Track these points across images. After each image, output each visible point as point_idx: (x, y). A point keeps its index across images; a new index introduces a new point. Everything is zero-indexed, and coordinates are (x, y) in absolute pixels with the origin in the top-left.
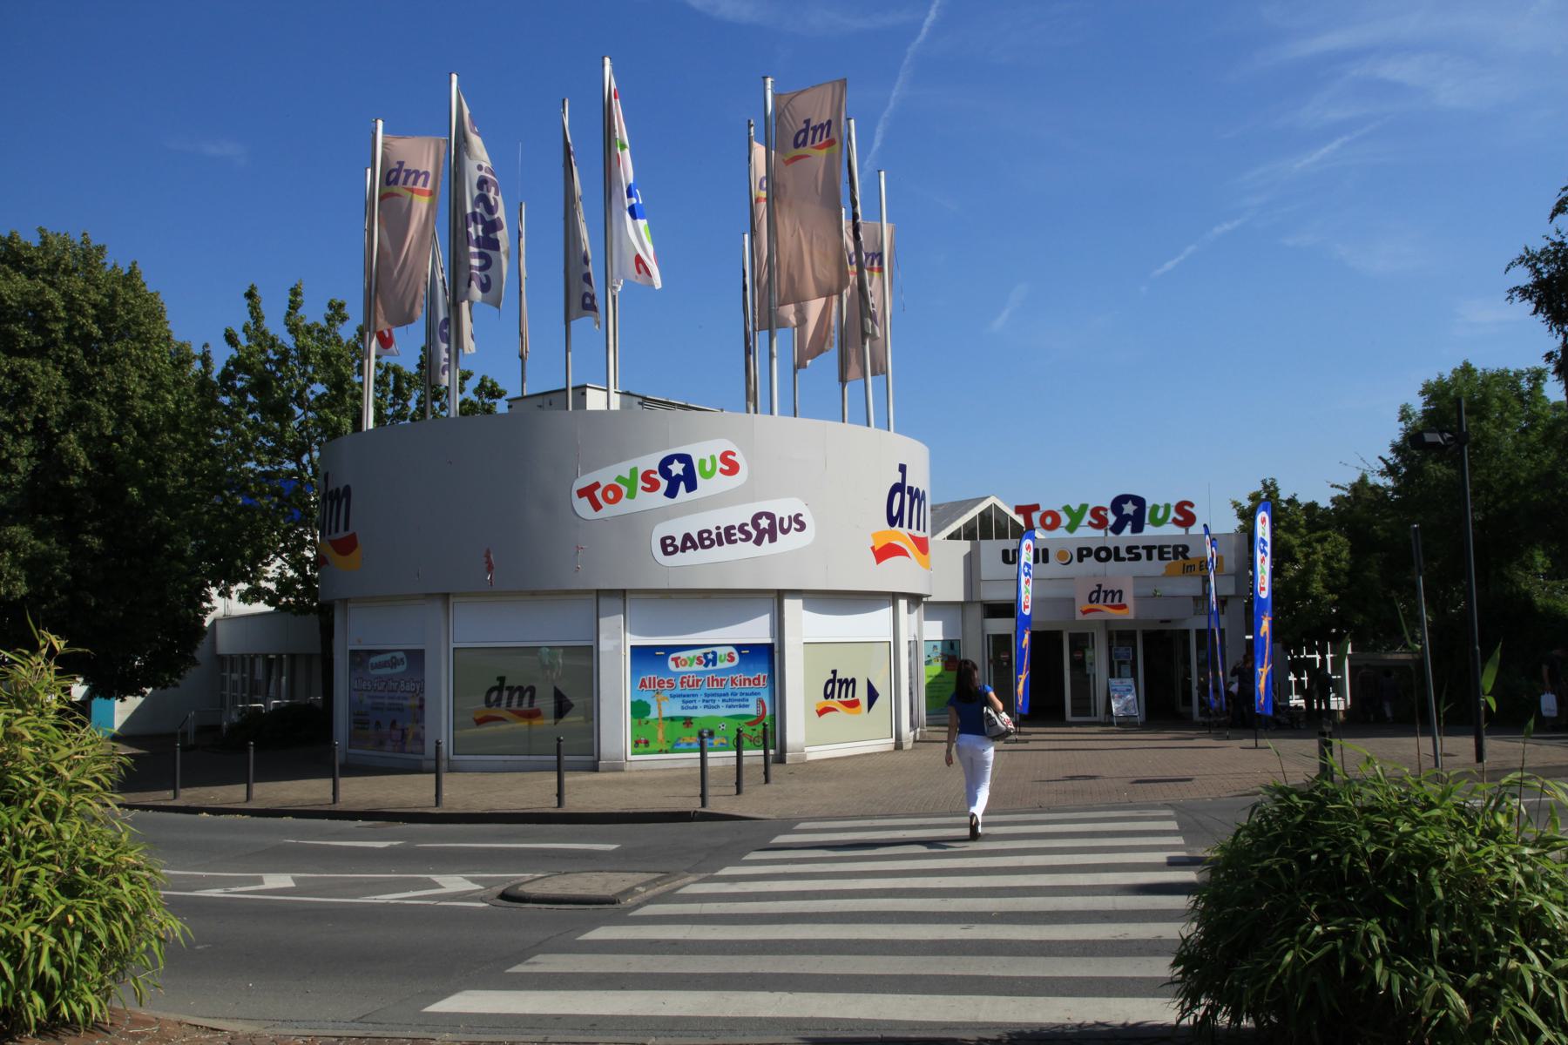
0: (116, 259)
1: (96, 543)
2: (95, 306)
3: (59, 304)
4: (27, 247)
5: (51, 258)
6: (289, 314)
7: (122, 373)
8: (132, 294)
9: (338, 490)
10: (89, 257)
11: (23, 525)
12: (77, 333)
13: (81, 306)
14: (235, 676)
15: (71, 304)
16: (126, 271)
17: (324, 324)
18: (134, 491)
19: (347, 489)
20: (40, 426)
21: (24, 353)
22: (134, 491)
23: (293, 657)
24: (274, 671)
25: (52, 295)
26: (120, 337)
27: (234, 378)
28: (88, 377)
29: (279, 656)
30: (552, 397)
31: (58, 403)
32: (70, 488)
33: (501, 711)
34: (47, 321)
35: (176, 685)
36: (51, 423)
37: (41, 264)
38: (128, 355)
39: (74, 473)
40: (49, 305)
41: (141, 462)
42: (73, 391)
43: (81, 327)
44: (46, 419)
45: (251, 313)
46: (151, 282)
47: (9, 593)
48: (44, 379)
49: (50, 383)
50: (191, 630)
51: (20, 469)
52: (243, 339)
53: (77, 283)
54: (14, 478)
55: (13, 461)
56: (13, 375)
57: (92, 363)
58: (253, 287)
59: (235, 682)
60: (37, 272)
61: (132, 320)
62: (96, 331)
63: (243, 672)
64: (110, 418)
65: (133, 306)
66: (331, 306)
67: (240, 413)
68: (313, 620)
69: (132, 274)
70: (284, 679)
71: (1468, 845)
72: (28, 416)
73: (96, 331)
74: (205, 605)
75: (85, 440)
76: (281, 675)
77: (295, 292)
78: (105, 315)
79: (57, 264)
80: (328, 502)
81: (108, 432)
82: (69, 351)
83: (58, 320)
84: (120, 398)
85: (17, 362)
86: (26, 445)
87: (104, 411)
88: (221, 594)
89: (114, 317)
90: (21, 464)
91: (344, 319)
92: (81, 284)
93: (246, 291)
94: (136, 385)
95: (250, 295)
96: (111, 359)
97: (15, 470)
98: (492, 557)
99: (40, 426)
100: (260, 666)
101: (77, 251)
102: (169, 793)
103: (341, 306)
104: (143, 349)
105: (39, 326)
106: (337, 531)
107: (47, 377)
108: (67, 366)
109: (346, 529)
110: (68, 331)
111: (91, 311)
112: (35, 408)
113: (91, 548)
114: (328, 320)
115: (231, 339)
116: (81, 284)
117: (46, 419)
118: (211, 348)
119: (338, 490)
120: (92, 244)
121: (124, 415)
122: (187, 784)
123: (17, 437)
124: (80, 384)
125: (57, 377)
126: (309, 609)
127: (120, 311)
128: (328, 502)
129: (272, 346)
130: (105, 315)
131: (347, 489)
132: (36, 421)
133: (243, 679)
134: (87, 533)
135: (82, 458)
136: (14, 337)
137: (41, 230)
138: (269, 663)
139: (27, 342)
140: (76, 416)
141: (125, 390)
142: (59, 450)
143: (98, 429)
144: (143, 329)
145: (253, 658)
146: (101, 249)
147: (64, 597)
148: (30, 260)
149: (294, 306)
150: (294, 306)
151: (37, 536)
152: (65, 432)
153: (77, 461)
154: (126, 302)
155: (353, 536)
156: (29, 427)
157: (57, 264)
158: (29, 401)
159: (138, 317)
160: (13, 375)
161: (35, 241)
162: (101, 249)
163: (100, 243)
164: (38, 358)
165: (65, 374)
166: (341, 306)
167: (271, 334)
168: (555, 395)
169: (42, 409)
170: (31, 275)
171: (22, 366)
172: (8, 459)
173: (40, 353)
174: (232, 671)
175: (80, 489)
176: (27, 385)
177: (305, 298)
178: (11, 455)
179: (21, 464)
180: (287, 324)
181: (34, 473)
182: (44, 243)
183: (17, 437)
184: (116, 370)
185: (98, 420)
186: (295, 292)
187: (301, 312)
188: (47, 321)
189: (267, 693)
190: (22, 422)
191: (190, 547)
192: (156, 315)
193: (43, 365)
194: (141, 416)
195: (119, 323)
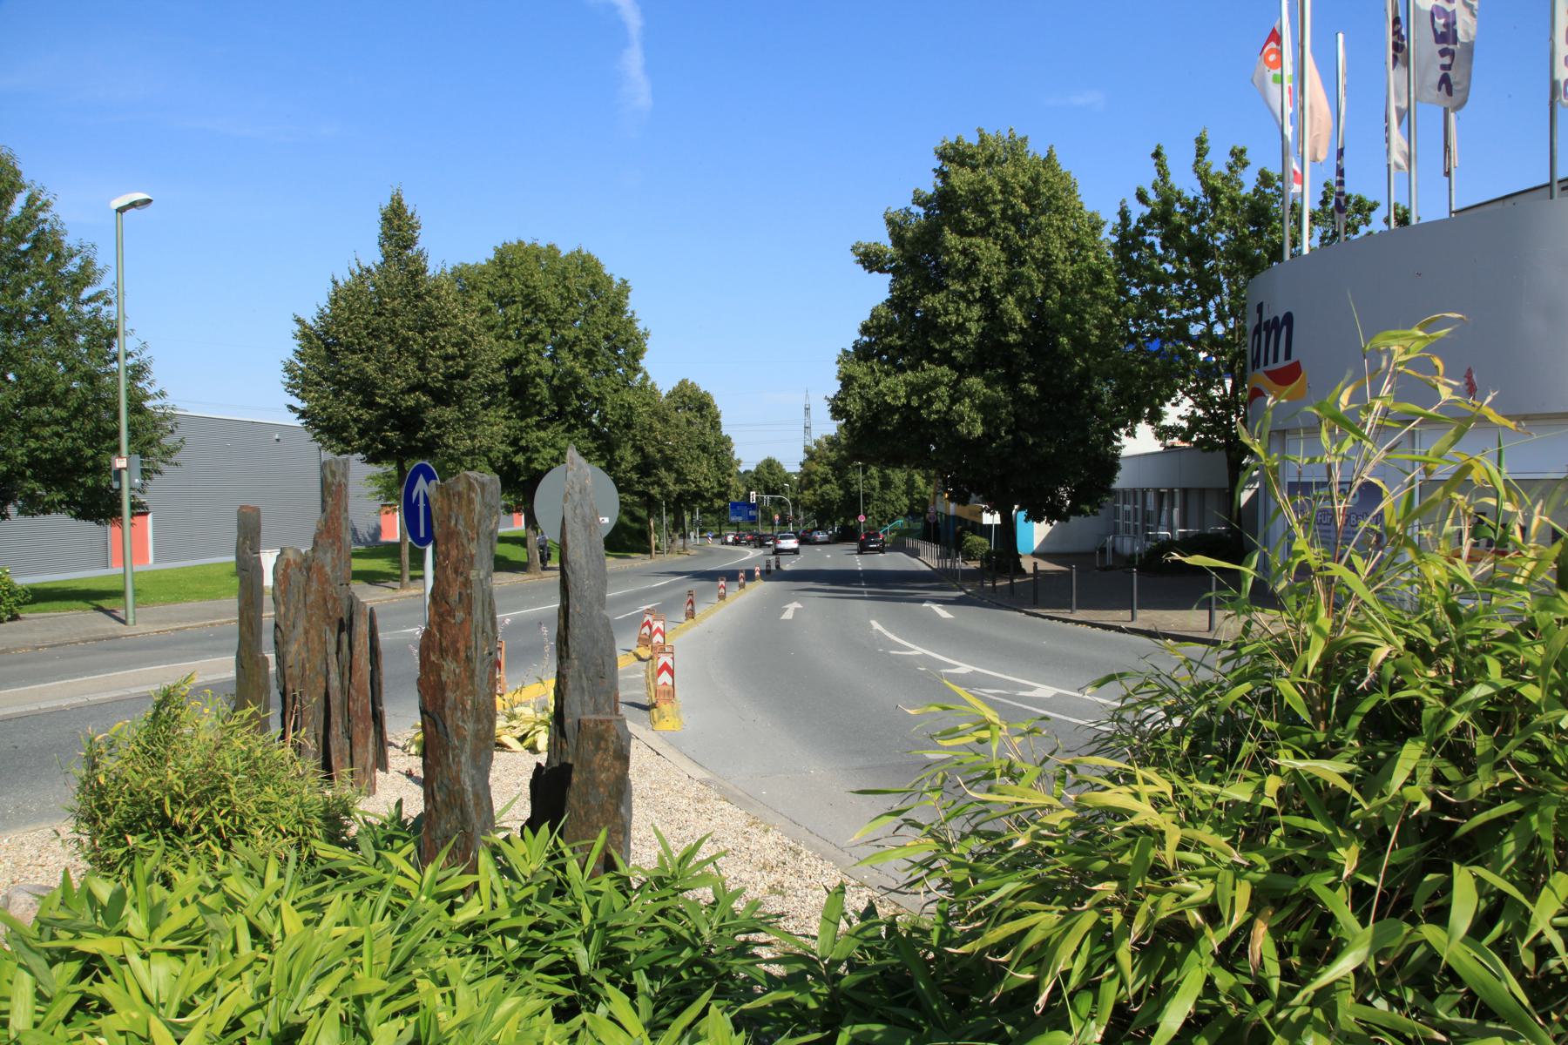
0: (1036, 149)
1: (1032, 389)
2: (1022, 187)
3: (997, 188)
4: (970, 146)
5: (988, 152)
6: (1197, 162)
7: (1046, 240)
8: (1051, 174)
9: (1276, 318)
10: (1015, 149)
11: (977, 376)
12: (1010, 212)
13: (1013, 188)
14: (1128, 507)
15: (1006, 188)
16: (1044, 155)
17: (1226, 172)
18: (1064, 340)
19: (1289, 318)
20: (986, 291)
21: (970, 234)
22: (1064, 340)
23: (1185, 491)
24: (1166, 502)
25: (990, 181)
26: (1043, 213)
27: (1144, 234)
28: (1020, 249)
29: (1171, 491)
30: (1515, 199)
31: (998, 273)
32: (1009, 345)
33: (1340, 548)
34: (988, 204)
35: (1095, 514)
36: (994, 290)
37: (981, 159)
38: (1051, 225)
39: (1012, 330)
40: (989, 190)
41: (1068, 316)
42: (1009, 262)
43: (1013, 207)
44: (990, 287)
45: (1159, 172)
46: (1065, 163)
47: (970, 433)
48: (987, 254)
49: (992, 256)
50: (1109, 464)
51: (973, 331)
52: (1152, 196)
53: (1008, 169)
54: (969, 338)
55: (615, 945)
56: (964, 252)
57: (1022, 237)
58: (1159, 147)
59: (1127, 513)
60: (978, 166)
61: (1052, 196)
62: (1025, 209)
63: (1135, 503)
64: (1039, 281)
65: (1053, 183)
66: (1233, 153)
67: (1152, 264)
68: (1221, 456)
69: (1050, 157)
70: (1176, 511)
71: (483, 464)
72: (976, 284)
73: (1025, 209)
74: (1116, 443)
75: (1020, 301)
76: (1172, 506)
77: (1200, 141)
78: (1031, 195)
79: (992, 156)
80: (1264, 334)
81: (1038, 294)
82: (1005, 228)
83: (996, 202)
84: (1045, 264)
85: (968, 240)
86: (976, 311)
87: (1034, 276)
88: (1128, 434)
89: (1038, 194)
90: (974, 328)
91: (1245, 165)
92: (1012, 170)
93: (1153, 151)
94: (1058, 250)
95: (1157, 155)
96: (1037, 231)
97: (968, 332)
98: (1474, 377)
99: (986, 291)
100: (1151, 498)
101: (1007, 145)
102: (1126, 614)
103: (1242, 152)
104: (1062, 220)
105: (982, 210)
106: (1276, 360)
107: (989, 251)
108: (1003, 241)
109: (1288, 356)
110: (1004, 211)
111: (1021, 192)
112: (981, 278)
113: (1028, 395)
114: (1230, 168)
115: (1142, 197)
116: (1012, 170)
117: (990, 287)
118: (1127, 203)
119: (1276, 318)
120: (1017, 137)
121: (1050, 278)
122: (1146, 605)
123: (970, 304)
124: (1014, 255)
125: (997, 252)
126: (1214, 447)
127: (1043, 189)
128: (1264, 334)
129: (1179, 200)
130: (1031, 195)
131: (1289, 318)
132: (982, 289)
133: (1135, 510)
134: (1025, 382)
135: (1019, 317)
136: (963, 221)
137: (979, 130)
138: (1160, 497)
139: (974, 224)
140: (1009, 286)
141: (1050, 256)
142: (1001, 311)
143: (1031, 292)
144: (1061, 203)
145: (1144, 492)
146: (1024, 140)
147: (1010, 437)
148: (972, 157)
149: (1201, 152)
150: (1201, 152)
151: (987, 386)
152: (1005, 297)
153: (1014, 319)
154: (1046, 182)
155: (1297, 364)
156: (978, 295)
157: (992, 156)
158: (976, 273)
159: (1057, 192)
160: (964, 252)
161: (975, 141)
162: (1024, 140)
163: (1023, 136)
164: (982, 237)
165: (1003, 249)
166: (1242, 152)
167: (1177, 189)
168: (1518, 198)
169: (987, 279)
170: (974, 168)
171: (970, 246)
172: (963, 324)
173: (983, 232)
174: (1125, 503)
175: (1017, 344)
176: (976, 260)
177: (1211, 144)
178: (966, 320)
179: (974, 328)
180: (1196, 172)
181: (981, 335)
182: (982, 141)
183: (970, 304)
184: (1042, 240)
185: (1030, 284)
186: (1200, 141)
187: (1208, 158)
188: (988, 204)
189: (1159, 523)
190: (972, 291)
191: (1106, 390)
192: (1070, 190)
193: (986, 242)
194: (1063, 279)
195: (1043, 200)
